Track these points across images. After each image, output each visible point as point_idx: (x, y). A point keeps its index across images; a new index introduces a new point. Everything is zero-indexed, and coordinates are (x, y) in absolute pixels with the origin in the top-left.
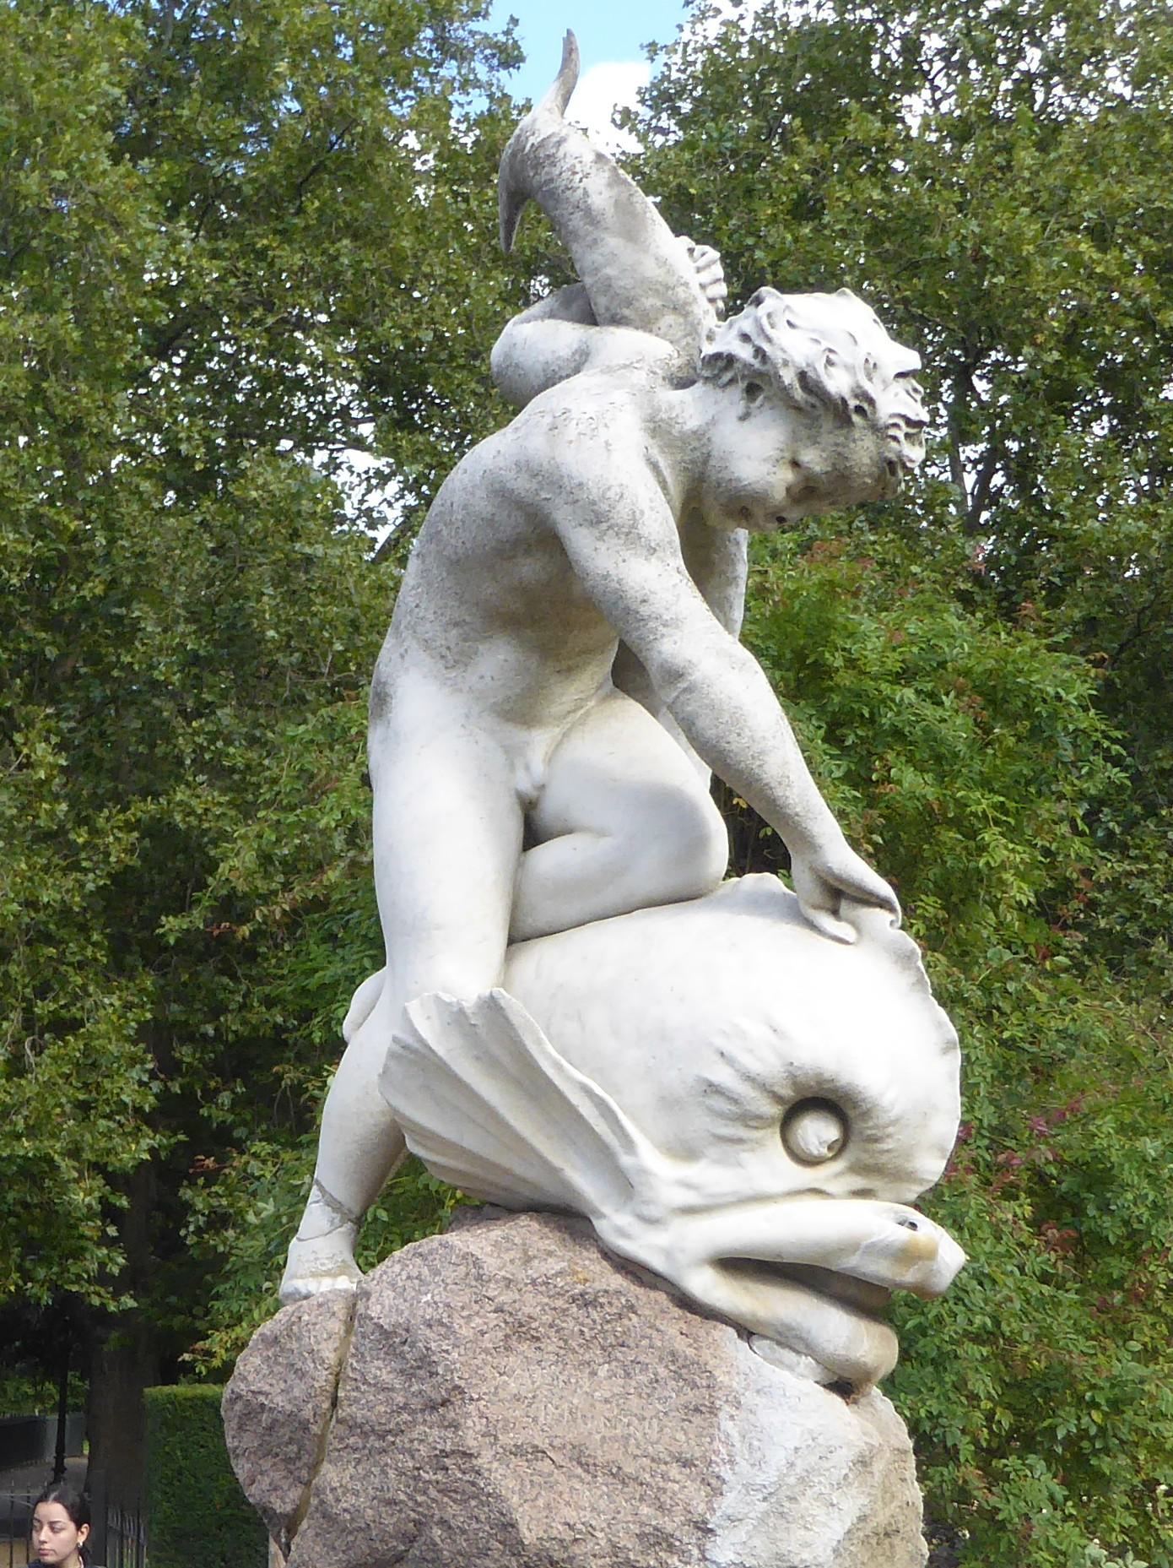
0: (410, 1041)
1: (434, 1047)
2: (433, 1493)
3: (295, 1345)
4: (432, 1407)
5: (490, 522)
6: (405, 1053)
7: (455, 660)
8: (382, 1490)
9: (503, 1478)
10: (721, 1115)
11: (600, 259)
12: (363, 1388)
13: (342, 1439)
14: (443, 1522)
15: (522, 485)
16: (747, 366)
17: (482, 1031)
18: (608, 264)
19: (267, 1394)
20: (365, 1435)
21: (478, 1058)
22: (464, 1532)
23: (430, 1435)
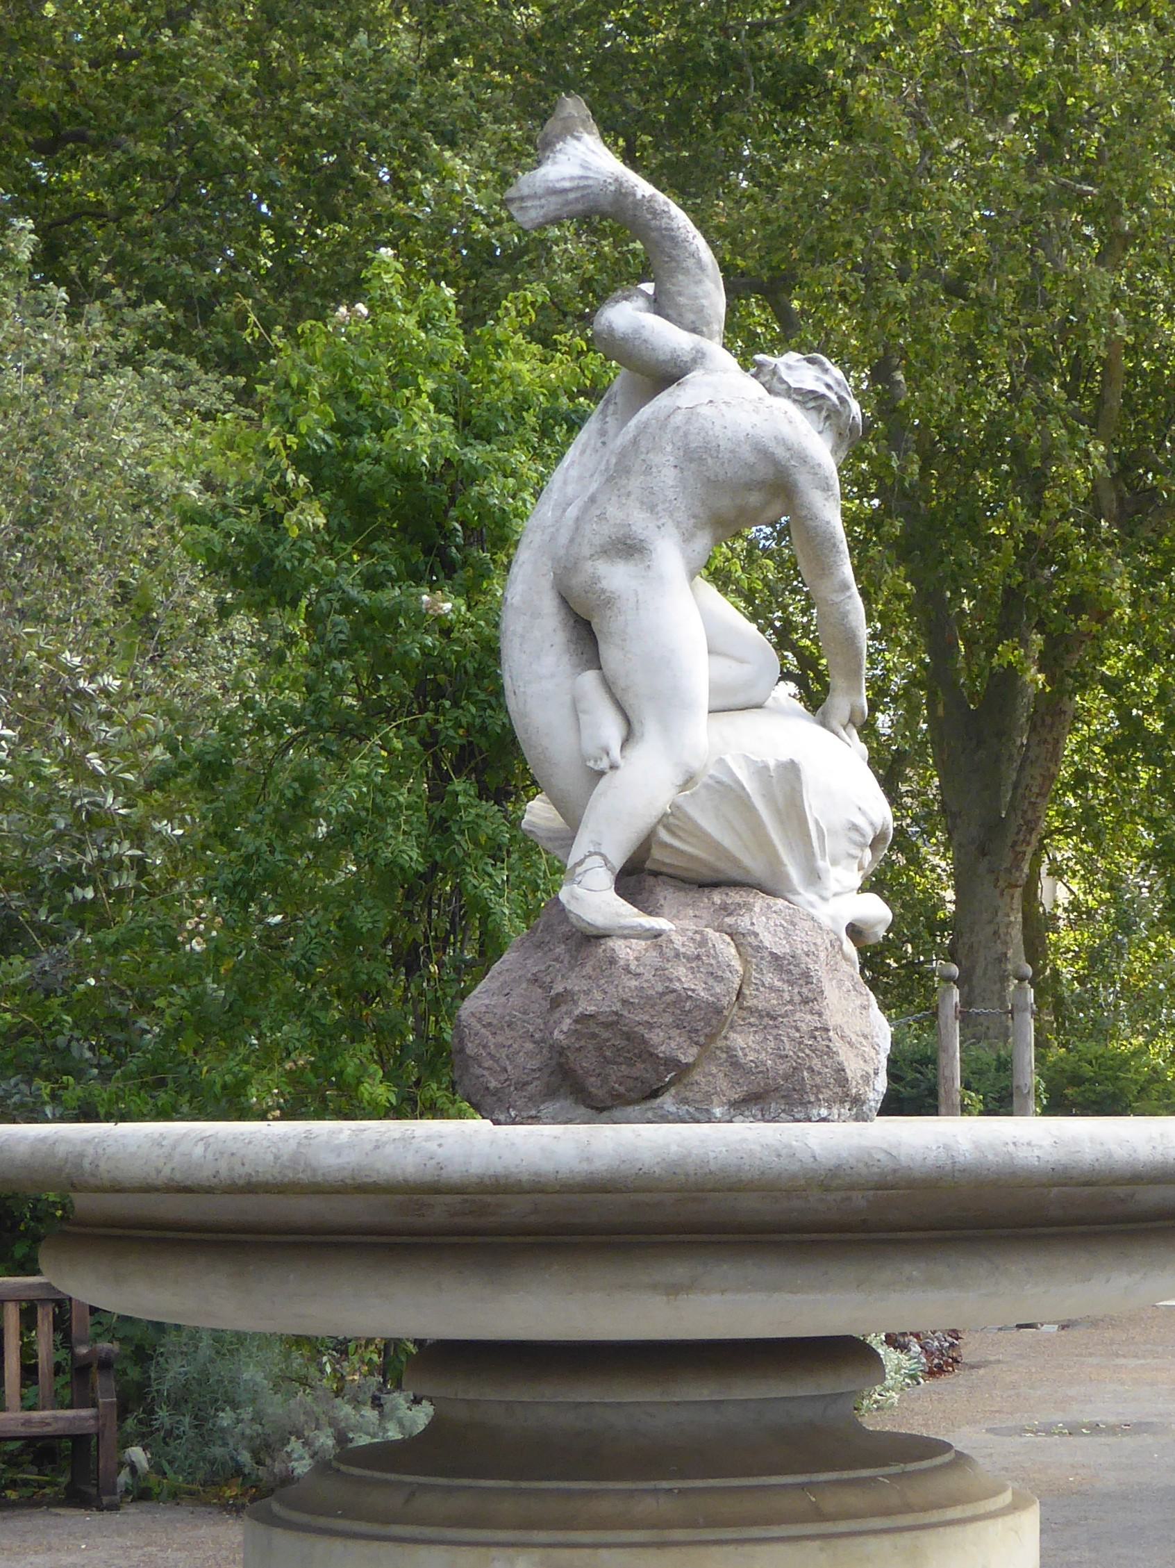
0: (725, 779)
1: (746, 786)
2: (807, 1051)
3: (713, 962)
4: (806, 1001)
5: (751, 467)
6: (717, 786)
7: (687, 538)
8: (779, 1049)
9: (837, 1044)
10: (855, 843)
11: (701, 293)
12: (762, 989)
13: (744, 1019)
14: (811, 1069)
15: (780, 452)
16: (834, 405)
17: (774, 780)
18: (705, 297)
19: (693, 991)
20: (761, 1017)
21: (764, 796)
22: (820, 1073)
23: (806, 1020)
